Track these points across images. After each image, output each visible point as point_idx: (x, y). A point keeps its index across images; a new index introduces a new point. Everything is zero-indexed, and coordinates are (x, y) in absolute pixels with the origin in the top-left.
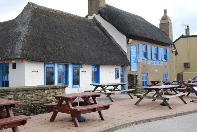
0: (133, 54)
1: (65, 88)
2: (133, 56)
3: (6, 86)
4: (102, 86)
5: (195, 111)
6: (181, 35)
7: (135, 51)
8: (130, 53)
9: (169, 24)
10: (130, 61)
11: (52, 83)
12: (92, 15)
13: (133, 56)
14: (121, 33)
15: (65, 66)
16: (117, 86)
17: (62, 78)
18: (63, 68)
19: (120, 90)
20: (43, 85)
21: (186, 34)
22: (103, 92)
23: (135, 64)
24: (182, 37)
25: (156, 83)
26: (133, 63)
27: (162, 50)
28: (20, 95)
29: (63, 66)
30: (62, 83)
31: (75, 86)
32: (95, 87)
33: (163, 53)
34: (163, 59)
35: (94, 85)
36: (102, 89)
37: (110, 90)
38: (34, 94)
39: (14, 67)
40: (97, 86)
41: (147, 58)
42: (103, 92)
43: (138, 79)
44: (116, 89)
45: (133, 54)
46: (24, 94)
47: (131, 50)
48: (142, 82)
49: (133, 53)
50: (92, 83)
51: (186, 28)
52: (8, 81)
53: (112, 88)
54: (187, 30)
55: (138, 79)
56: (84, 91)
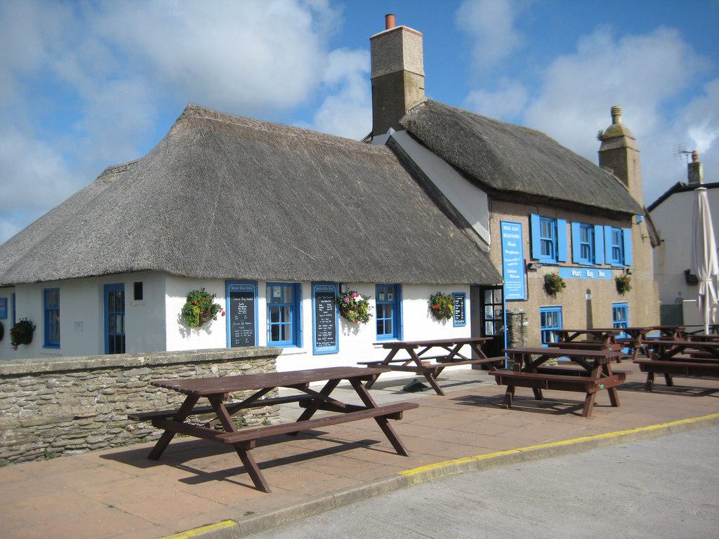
0: (510, 249)
1: (275, 357)
2: (512, 252)
3: (118, 352)
4: (410, 347)
5: (3, 376)
6: (673, 184)
7: (518, 236)
8: (500, 246)
9: (628, 150)
10: (500, 269)
11: (251, 341)
12: (385, 131)
13: (512, 252)
14: (472, 183)
15: (290, 288)
16: (460, 343)
17: (283, 326)
18: (285, 295)
19: (470, 358)
20: (219, 350)
21: (690, 178)
22: (413, 364)
23: (518, 277)
24: (678, 188)
25: (570, 334)
26: (511, 276)
27: (604, 234)
28: (132, 380)
29: (536, 219)
30: (283, 339)
31: (321, 349)
32: (389, 351)
33: (610, 245)
34: (610, 259)
35: (386, 346)
36: (409, 357)
37: (439, 359)
38: (176, 376)
39: (138, 295)
40: (395, 348)
41: (557, 258)
42: (413, 364)
43: (525, 323)
44: (456, 357)
45: (510, 249)
46: (146, 375)
47: (505, 235)
48: (542, 332)
49: (510, 244)
50: (378, 339)
51: (690, 161)
52: (124, 337)
53: (443, 352)
54: (694, 168)
55: (525, 323)
56: (358, 363)
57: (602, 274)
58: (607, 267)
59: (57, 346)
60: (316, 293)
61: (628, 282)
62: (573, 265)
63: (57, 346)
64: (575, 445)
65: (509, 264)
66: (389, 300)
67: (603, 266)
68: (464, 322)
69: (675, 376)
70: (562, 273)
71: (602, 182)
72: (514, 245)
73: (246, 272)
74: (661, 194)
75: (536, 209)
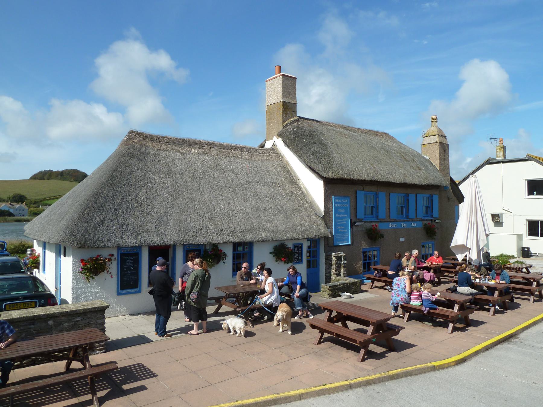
6: (486, 159)
26: (340, 231)
57: (413, 224)
58: (418, 220)
59: (530, 193)
60: (186, 250)
61: (200, 262)
62: (391, 220)
63: (530, 193)
64: (12, 278)
65: (339, 223)
66: (245, 250)
67: (416, 220)
68: (301, 262)
69: (459, 306)
70: (382, 227)
71: (417, 167)
72: (343, 211)
73: (425, 154)
74: (479, 165)
75: (362, 187)
